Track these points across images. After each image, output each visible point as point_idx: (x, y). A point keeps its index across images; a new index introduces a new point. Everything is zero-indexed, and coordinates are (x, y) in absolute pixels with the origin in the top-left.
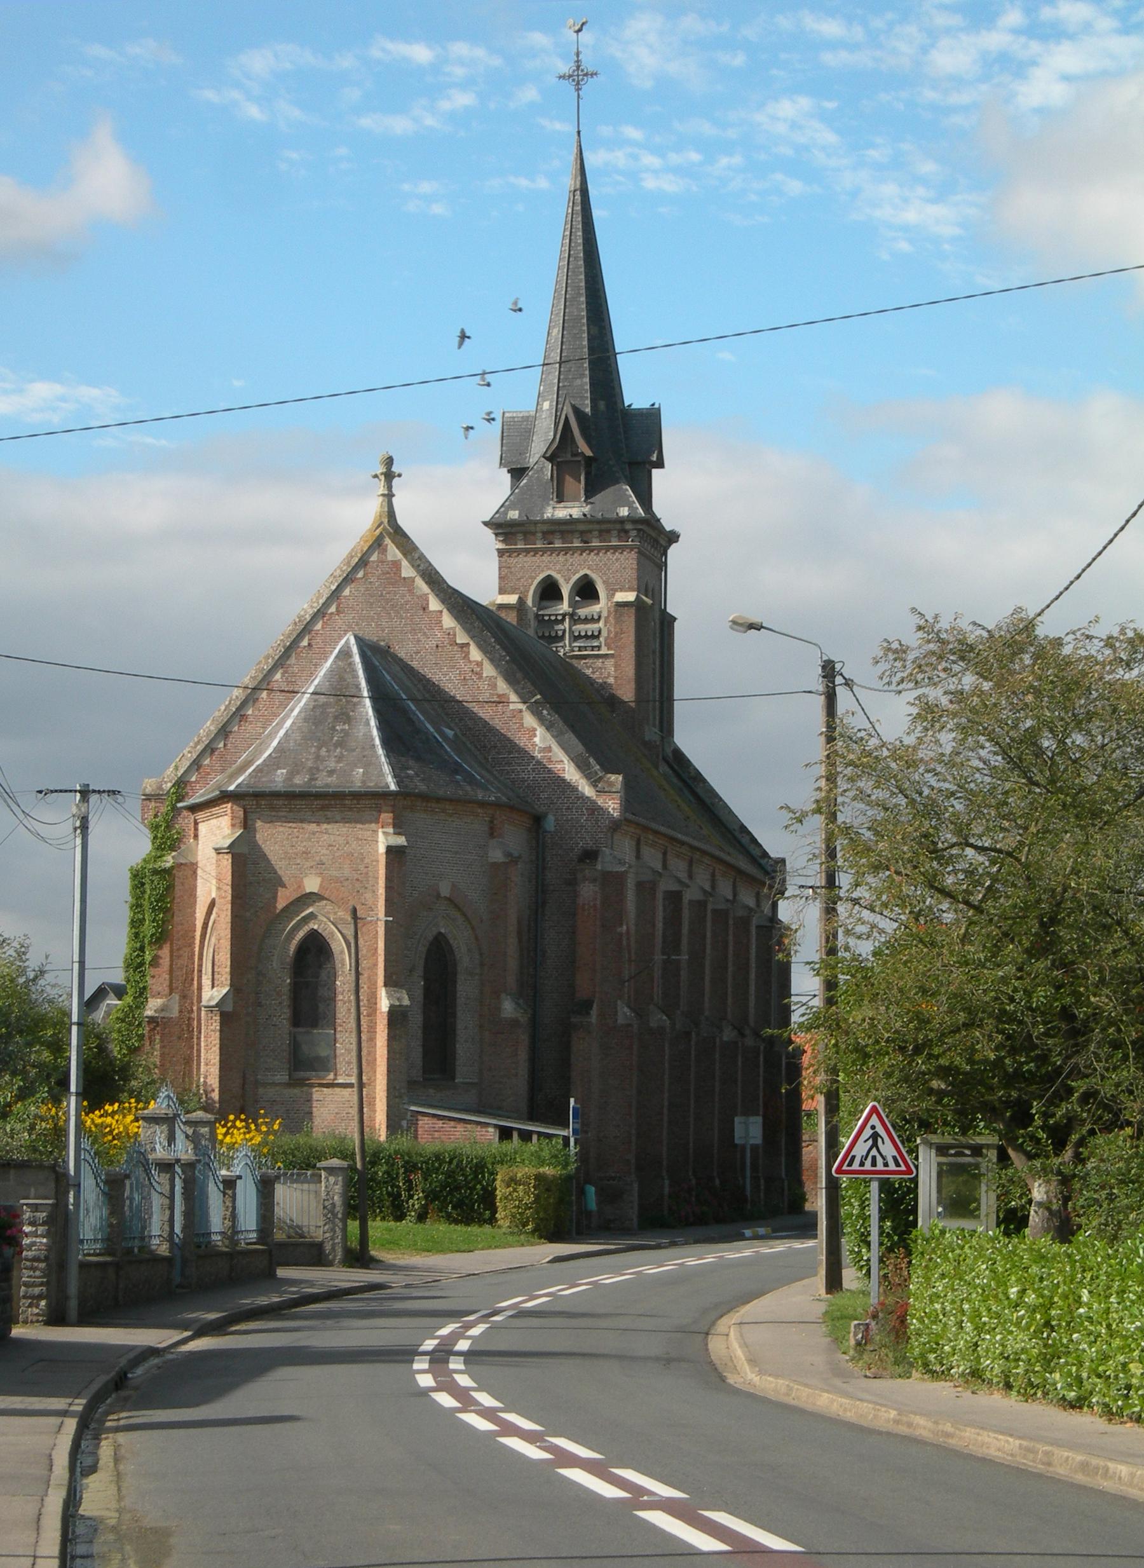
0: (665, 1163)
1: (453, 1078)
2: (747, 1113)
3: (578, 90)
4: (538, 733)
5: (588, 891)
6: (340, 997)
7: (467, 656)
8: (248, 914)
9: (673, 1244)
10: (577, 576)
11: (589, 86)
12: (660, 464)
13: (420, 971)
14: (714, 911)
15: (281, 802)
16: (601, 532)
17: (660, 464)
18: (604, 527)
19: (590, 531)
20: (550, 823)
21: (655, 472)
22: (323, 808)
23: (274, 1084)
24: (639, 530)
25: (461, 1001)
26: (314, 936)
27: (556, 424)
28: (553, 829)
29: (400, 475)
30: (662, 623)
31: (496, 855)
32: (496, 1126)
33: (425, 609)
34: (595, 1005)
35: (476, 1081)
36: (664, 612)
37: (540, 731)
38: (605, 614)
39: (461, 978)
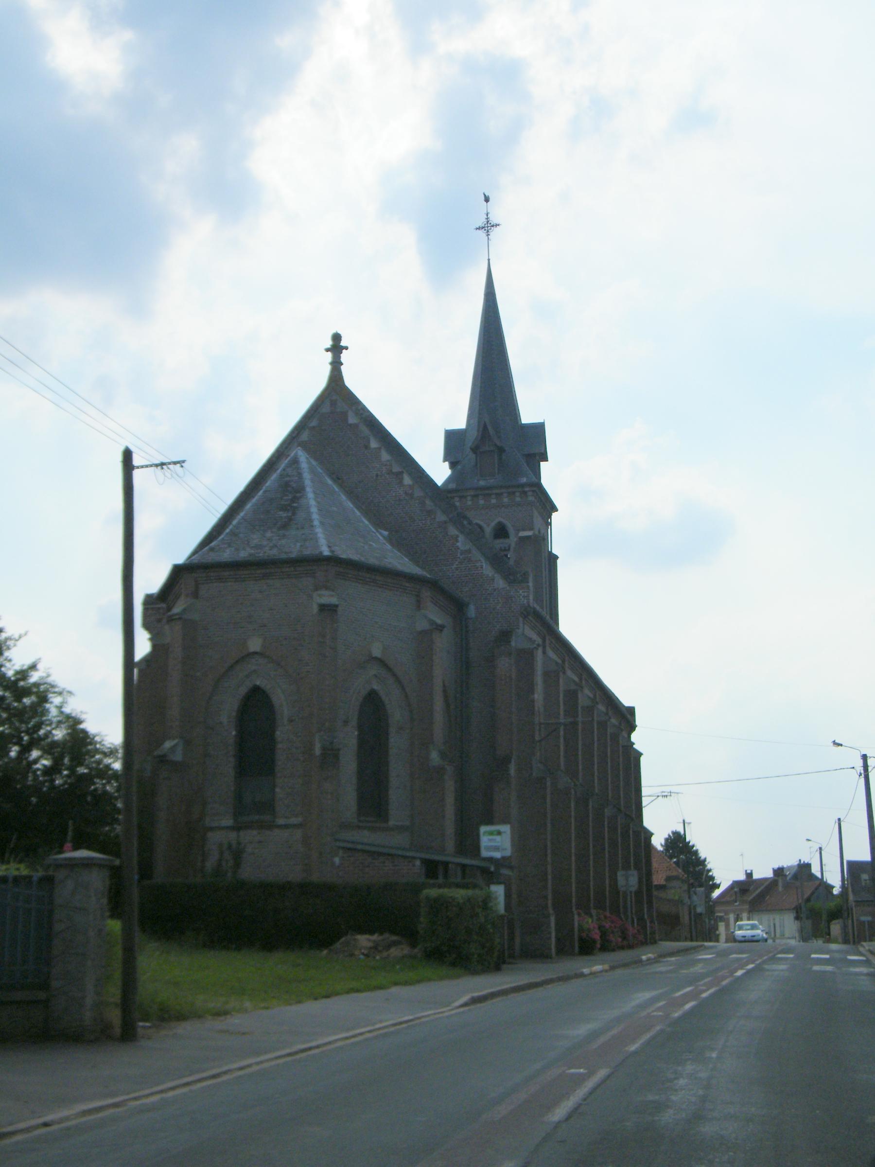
0: (574, 900)
1: (387, 821)
2: (626, 867)
3: (488, 235)
4: (460, 539)
5: (505, 665)
6: (279, 746)
7: (401, 482)
8: (198, 674)
9: (441, 978)
10: (493, 524)
11: (494, 232)
12: (545, 459)
13: (354, 722)
14: (599, 723)
15: (227, 573)
16: (509, 493)
17: (545, 459)
18: (510, 490)
19: (502, 494)
20: (472, 611)
21: (543, 464)
22: (265, 576)
23: (220, 828)
24: (533, 491)
25: (393, 752)
26: (256, 691)
27: (479, 425)
28: (473, 616)
29: (346, 348)
30: (549, 560)
31: (422, 625)
32: (421, 859)
33: (367, 447)
34: (513, 761)
35: (407, 823)
36: (550, 553)
37: (461, 538)
38: (513, 545)
39: (392, 730)
